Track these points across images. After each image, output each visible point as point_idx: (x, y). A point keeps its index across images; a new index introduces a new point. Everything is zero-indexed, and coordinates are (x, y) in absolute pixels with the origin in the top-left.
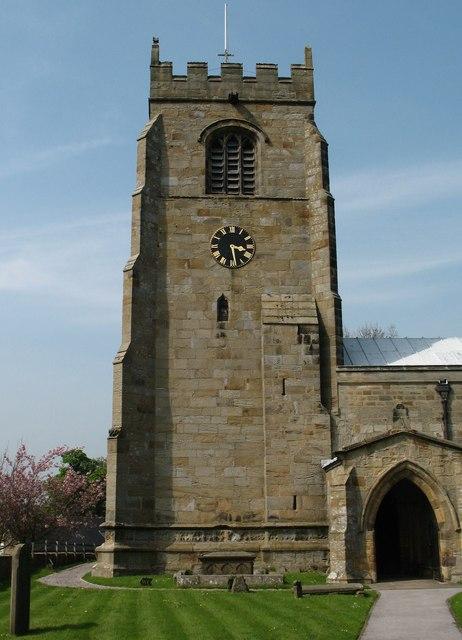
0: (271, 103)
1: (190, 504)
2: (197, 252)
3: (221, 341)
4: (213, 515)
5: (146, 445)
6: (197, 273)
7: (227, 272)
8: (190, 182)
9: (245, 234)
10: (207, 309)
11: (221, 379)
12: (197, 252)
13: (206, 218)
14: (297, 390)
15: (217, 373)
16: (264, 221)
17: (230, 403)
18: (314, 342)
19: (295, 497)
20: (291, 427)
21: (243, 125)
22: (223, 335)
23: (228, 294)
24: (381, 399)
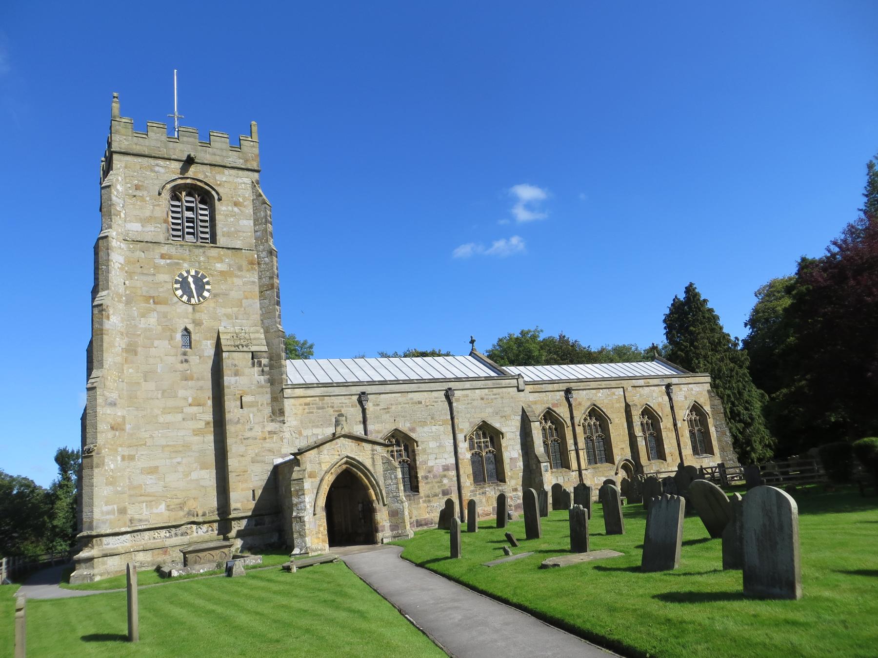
0: (224, 167)
1: (161, 507)
2: (161, 290)
3: (185, 365)
4: (181, 513)
5: (119, 458)
6: (161, 308)
7: (190, 308)
8: (153, 229)
9: (204, 277)
10: (171, 338)
11: (186, 399)
12: (161, 290)
13: (168, 261)
14: (252, 405)
15: (181, 393)
16: (219, 266)
17: (193, 418)
18: (265, 366)
19: (253, 491)
20: (248, 434)
21: (199, 183)
22: (186, 361)
23: (190, 327)
24: (318, 408)
